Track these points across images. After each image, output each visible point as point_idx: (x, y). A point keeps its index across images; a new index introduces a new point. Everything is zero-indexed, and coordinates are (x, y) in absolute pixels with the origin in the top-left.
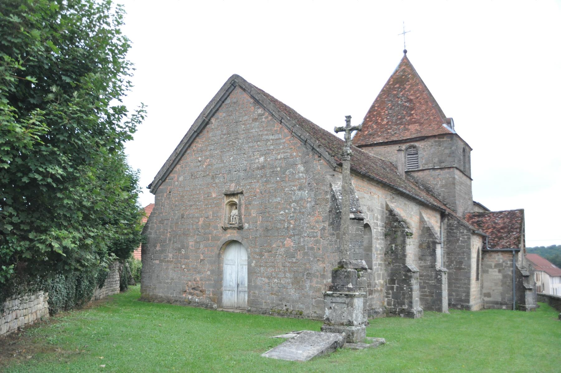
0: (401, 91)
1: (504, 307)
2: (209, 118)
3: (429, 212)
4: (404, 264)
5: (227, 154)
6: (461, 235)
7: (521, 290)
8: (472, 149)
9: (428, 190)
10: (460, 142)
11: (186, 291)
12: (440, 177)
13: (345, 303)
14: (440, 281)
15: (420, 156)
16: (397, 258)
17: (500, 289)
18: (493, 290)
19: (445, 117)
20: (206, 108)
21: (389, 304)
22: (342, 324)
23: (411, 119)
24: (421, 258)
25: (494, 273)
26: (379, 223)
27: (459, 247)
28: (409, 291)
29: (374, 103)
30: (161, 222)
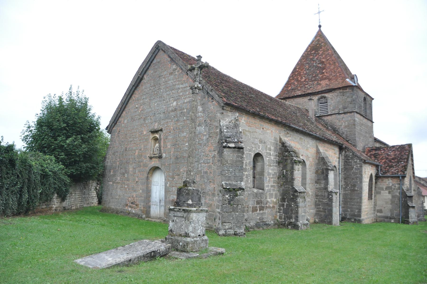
0: (316, 56)
1: (392, 221)
2: (142, 75)
3: (327, 145)
4: (292, 186)
5: (153, 101)
6: (355, 164)
7: (406, 208)
8: (373, 99)
9: (335, 131)
10: (360, 92)
11: (127, 205)
12: (343, 120)
13: (183, 217)
14: (331, 200)
15: (329, 104)
16: (288, 181)
17: (390, 206)
18: (384, 208)
19: (351, 73)
20: (140, 67)
21: (280, 218)
22: (180, 235)
23: (322, 77)
24: (317, 182)
25: (385, 194)
26: (272, 153)
27: (354, 173)
28: (296, 208)
29: (296, 66)
30: (114, 154)
